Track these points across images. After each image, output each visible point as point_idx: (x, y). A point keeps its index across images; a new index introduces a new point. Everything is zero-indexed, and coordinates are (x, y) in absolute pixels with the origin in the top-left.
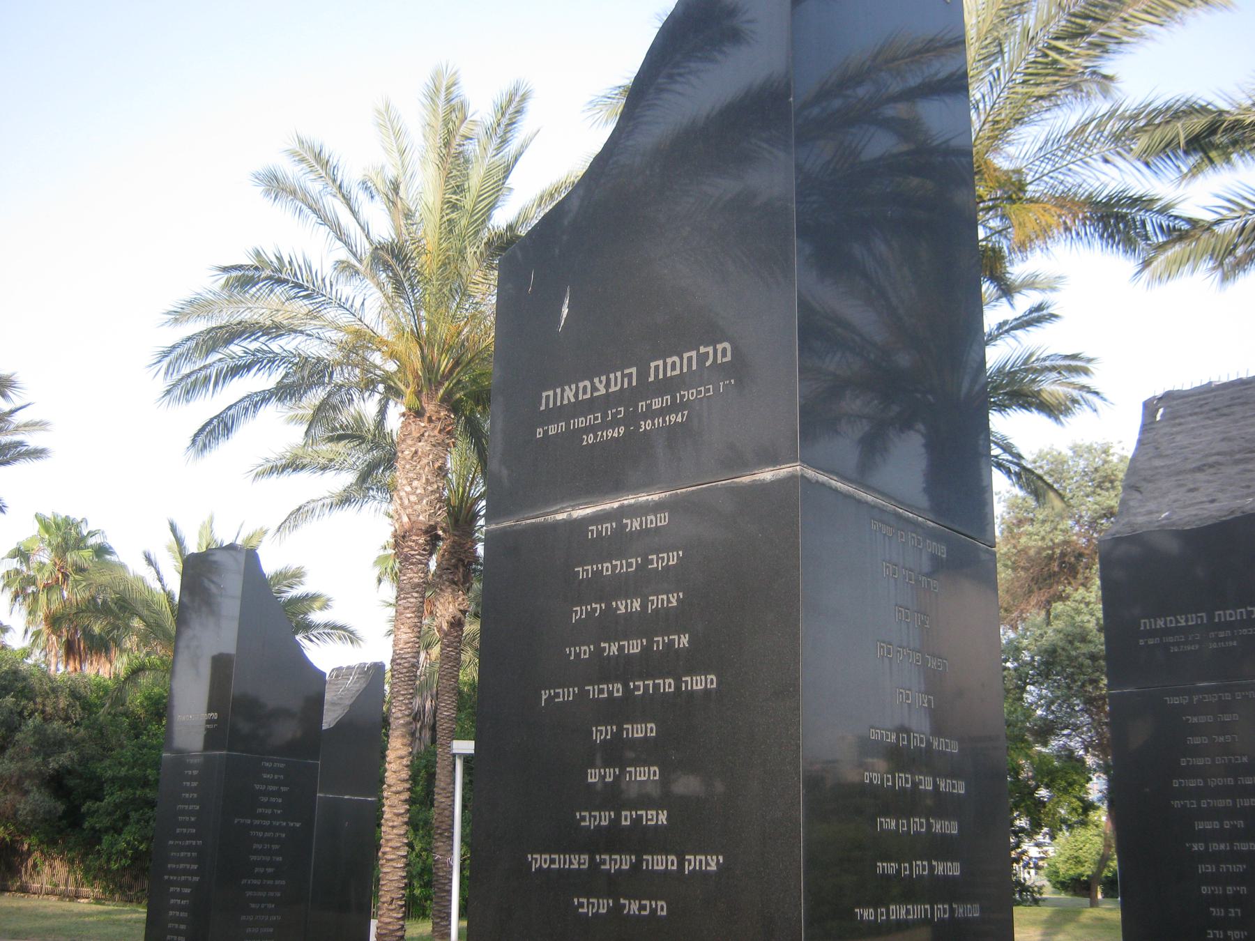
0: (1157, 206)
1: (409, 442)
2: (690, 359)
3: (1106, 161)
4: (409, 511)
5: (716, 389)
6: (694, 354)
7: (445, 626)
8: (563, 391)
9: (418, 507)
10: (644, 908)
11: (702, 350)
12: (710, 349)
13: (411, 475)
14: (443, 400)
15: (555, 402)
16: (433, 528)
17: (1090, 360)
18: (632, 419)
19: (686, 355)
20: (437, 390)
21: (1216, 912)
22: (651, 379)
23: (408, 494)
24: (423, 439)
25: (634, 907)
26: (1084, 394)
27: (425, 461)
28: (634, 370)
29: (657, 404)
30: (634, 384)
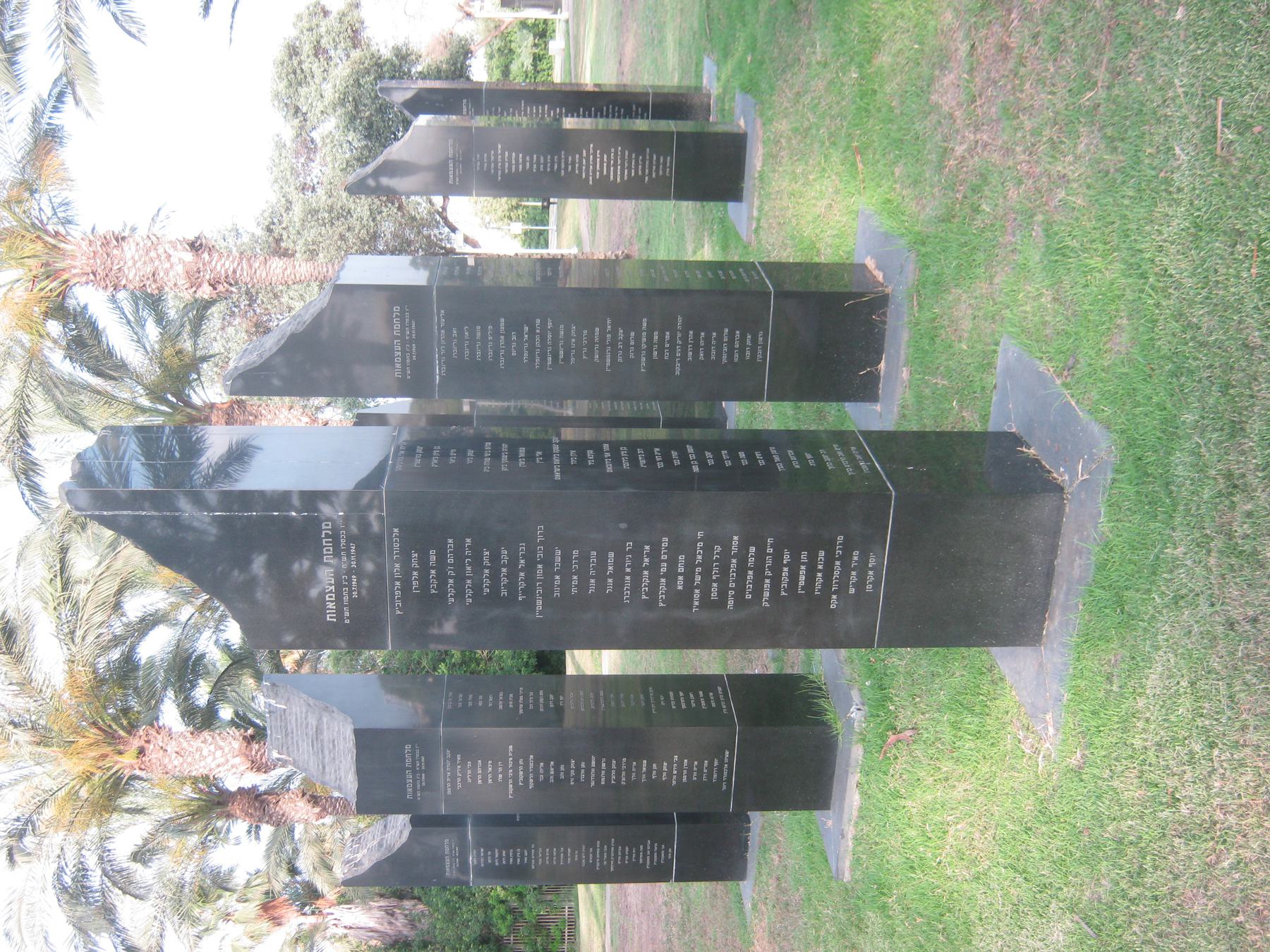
0: (40, 106)
1: (167, 760)
3: (11, 121)
4: (229, 756)
7: (317, 810)
9: (226, 750)
13: (197, 756)
14: (129, 733)
16: (245, 738)
17: (125, 225)
20: (120, 737)
21: (542, 777)
23: (215, 759)
25: (699, 557)
26: (159, 219)
27: (185, 745)
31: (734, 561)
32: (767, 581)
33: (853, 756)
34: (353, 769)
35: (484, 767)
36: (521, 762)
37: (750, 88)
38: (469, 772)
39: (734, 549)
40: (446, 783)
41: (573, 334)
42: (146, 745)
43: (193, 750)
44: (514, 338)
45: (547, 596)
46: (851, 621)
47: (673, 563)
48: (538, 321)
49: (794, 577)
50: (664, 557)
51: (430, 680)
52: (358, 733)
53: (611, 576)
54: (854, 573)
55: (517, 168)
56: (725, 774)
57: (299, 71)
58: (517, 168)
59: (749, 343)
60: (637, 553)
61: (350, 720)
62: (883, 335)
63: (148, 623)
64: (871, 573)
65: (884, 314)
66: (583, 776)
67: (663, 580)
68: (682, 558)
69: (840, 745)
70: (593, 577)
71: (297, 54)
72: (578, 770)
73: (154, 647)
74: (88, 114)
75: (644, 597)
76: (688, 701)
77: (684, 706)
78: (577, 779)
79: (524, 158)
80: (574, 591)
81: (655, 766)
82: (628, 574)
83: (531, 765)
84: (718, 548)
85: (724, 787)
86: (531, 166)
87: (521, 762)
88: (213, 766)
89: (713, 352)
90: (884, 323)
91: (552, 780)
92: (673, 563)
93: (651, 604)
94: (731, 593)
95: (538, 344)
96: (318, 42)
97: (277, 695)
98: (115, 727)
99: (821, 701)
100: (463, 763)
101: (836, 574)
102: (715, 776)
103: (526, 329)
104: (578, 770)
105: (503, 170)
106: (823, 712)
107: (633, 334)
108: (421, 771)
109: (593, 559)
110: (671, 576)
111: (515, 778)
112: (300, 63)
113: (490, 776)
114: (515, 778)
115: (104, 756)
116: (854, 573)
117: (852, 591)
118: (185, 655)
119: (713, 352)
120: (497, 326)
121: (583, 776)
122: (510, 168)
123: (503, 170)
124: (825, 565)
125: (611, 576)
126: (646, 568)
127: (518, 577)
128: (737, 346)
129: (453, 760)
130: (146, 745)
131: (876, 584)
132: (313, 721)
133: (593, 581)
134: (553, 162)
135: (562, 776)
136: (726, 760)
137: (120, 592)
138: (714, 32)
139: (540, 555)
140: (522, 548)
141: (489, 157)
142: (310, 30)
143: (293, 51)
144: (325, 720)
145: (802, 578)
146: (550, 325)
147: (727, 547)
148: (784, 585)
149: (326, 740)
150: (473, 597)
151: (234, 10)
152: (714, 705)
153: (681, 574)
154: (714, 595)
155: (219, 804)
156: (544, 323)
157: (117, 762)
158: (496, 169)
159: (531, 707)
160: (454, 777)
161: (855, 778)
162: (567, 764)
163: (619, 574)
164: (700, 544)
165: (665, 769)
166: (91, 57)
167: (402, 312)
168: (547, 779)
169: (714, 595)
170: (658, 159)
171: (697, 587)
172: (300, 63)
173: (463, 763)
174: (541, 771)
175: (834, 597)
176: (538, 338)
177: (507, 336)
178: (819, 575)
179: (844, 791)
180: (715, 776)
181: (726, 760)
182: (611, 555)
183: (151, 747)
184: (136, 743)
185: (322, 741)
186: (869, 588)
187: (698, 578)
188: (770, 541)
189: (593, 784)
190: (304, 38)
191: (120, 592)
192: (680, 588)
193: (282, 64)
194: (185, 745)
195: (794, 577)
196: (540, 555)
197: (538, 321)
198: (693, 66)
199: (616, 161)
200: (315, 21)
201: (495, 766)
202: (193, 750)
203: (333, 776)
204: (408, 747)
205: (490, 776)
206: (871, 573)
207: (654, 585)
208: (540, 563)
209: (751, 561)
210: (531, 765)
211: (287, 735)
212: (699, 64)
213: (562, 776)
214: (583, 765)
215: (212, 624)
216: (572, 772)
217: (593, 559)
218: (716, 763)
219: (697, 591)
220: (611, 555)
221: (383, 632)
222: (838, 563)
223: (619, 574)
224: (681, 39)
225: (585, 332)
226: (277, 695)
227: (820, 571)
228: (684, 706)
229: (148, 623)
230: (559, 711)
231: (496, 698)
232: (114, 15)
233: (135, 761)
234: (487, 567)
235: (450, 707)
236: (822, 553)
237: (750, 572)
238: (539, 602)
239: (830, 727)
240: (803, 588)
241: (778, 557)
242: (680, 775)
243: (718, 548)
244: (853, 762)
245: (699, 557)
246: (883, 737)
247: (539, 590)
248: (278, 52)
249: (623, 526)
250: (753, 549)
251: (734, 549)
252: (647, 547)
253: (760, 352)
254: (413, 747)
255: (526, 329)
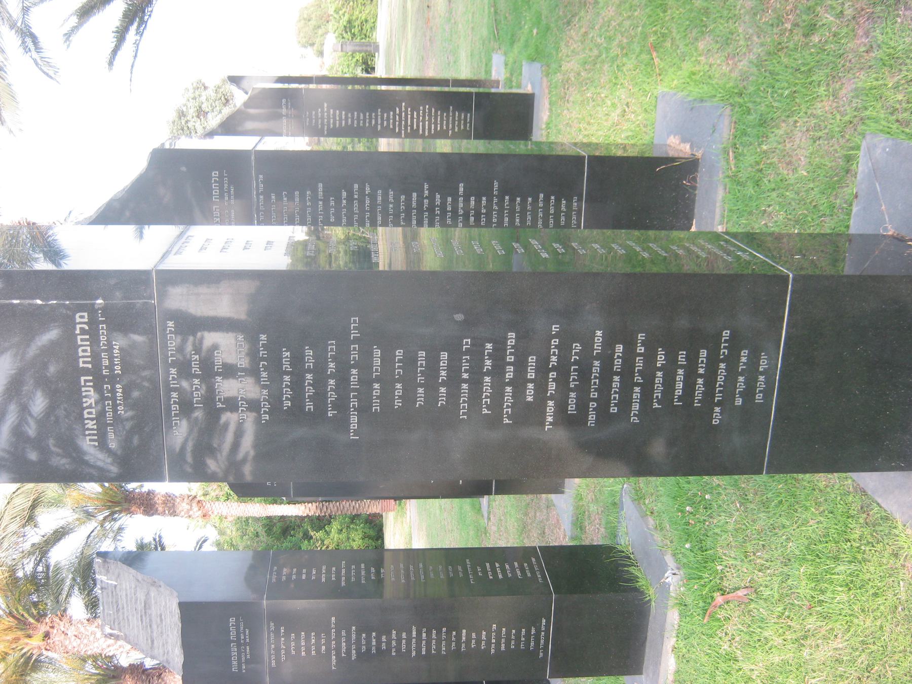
1: (67, 642)
2: (82, 340)
5: (103, 322)
6: (79, 337)
8: (88, 429)
10: (554, 352)
11: (78, 332)
12: (78, 326)
13: (92, 638)
14: (38, 620)
15: (94, 435)
18: (113, 379)
19: (79, 343)
20: (30, 624)
21: (364, 648)
22: (90, 366)
24: (66, 631)
25: (554, 358)
27: (82, 629)
28: (83, 378)
29: (106, 362)
30: (91, 378)
31: (597, 363)
32: (637, 389)
33: (669, 620)
34: (179, 643)
35: (308, 638)
36: (343, 633)
37: (538, 55)
38: (293, 644)
39: (597, 348)
40: (270, 655)
41: (391, 199)
42: (51, 630)
43: (89, 634)
44: (332, 203)
45: (364, 409)
46: (737, 440)
47: (520, 366)
48: (356, 186)
49: (669, 383)
50: (510, 359)
51: (292, 586)
52: (182, 605)
53: (444, 384)
54: (741, 379)
55: (341, 124)
56: (542, 641)
57: (185, 128)
58: (341, 124)
59: (563, 208)
60: (477, 353)
61: (176, 594)
62: (693, 201)
63: (59, 535)
64: (762, 378)
65: (694, 179)
66: (404, 647)
67: (509, 389)
68: (532, 359)
69: (653, 611)
70: (421, 386)
71: (184, 116)
72: (399, 641)
73: (63, 555)
74: (11, 131)
75: (485, 411)
76: (504, 571)
77: (500, 576)
78: (398, 650)
79: (346, 115)
80: (398, 403)
81: (474, 635)
82: (465, 381)
83: (354, 636)
84: (577, 347)
85: (541, 655)
86: (353, 122)
87: (343, 633)
88: (104, 646)
89: (529, 218)
90: (695, 188)
91: (374, 651)
92: (520, 366)
93: (494, 421)
94: (592, 405)
95: (356, 209)
96: (200, 107)
97: (108, 571)
98: (26, 615)
99: (631, 569)
100: (287, 635)
101: (720, 379)
102: (532, 644)
103: (344, 194)
104: (399, 641)
105: (329, 125)
106: (635, 579)
107: (449, 199)
108: (245, 644)
109: (421, 362)
110: (519, 383)
111: (338, 650)
112: (187, 122)
113: (313, 648)
114: (338, 650)
115: (17, 640)
116: (741, 379)
117: (739, 402)
118: (88, 561)
119: (529, 218)
120: (315, 191)
121: (404, 647)
122: (334, 123)
123: (329, 125)
124: (707, 368)
125: (444, 384)
126: (488, 373)
127: (326, 385)
128: (552, 211)
129: (277, 632)
130: (51, 630)
131: (768, 393)
132: (141, 596)
133: (421, 390)
134: (371, 118)
135: (384, 646)
136: (543, 628)
137: (33, 507)
138: (502, 31)
139: (354, 355)
140: (332, 347)
141: (316, 114)
142: (194, 98)
143: (182, 114)
144: (152, 595)
145: (680, 385)
146: (368, 190)
147: (588, 345)
148: (657, 394)
149: (154, 614)
150: (270, 413)
151: (132, 67)
152: (529, 575)
153: (531, 381)
154: (572, 409)
155: (114, 677)
156: (362, 190)
157: (27, 644)
158: (322, 124)
159: (353, 579)
160: (278, 650)
161: (670, 642)
162: (389, 634)
163: (454, 381)
164: (555, 342)
165: (484, 637)
166: (13, 87)
167: (221, 177)
168: (369, 650)
169: (572, 409)
170: (460, 116)
171: (551, 398)
172: (187, 122)
173: (287, 635)
174: (364, 642)
175: (717, 409)
176: (356, 203)
177: (326, 201)
178: (700, 381)
179: (659, 655)
180: (532, 644)
181: (543, 628)
182: (444, 355)
183: (55, 631)
184: (43, 628)
185: (150, 615)
186: (759, 398)
187: (552, 386)
188: (641, 337)
189: (414, 654)
190: (189, 104)
191: (33, 507)
192: (530, 399)
193: (174, 122)
194: (82, 629)
195: (669, 383)
196: (354, 355)
197: (356, 186)
198: (484, 66)
199: (424, 117)
200: (197, 93)
201: (318, 637)
202: (89, 634)
203: (161, 651)
204: (232, 621)
205: (313, 648)
206: (762, 378)
207: (497, 397)
208: (354, 367)
209: (618, 363)
210: (354, 636)
211: (118, 611)
212: (490, 60)
213: (384, 646)
214: (404, 635)
215: (111, 535)
216: (394, 643)
217: (421, 362)
218: (533, 631)
219: (551, 403)
220: (444, 355)
221: (160, 467)
222: (722, 366)
223: (454, 381)
224: (472, 52)
225: (403, 197)
226: (108, 571)
227: (701, 376)
228: (500, 576)
229: (59, 535)
230: (380, 581)
231: (319, 572)
232: (35, 61)
233: (41, 643)
234: (287, 373)
235: (274, 580)
236: (704, 353)
237: (616, 378)
238: (354, 419)
239: (642, 593)
240: (680, 398)
241: (650, 358)
242: (498, 644)
243: (577, 347)
244: (668, 626)
245: (554, 358)
246: (708, 600)
247: (354, 403)
248: (173, 116)
249: (459, 317)
250: (620, 348)
251: (597, 348)
252: (489, 346)
253: (574, 217)
254: (237, 621)
255: (344, 194)
